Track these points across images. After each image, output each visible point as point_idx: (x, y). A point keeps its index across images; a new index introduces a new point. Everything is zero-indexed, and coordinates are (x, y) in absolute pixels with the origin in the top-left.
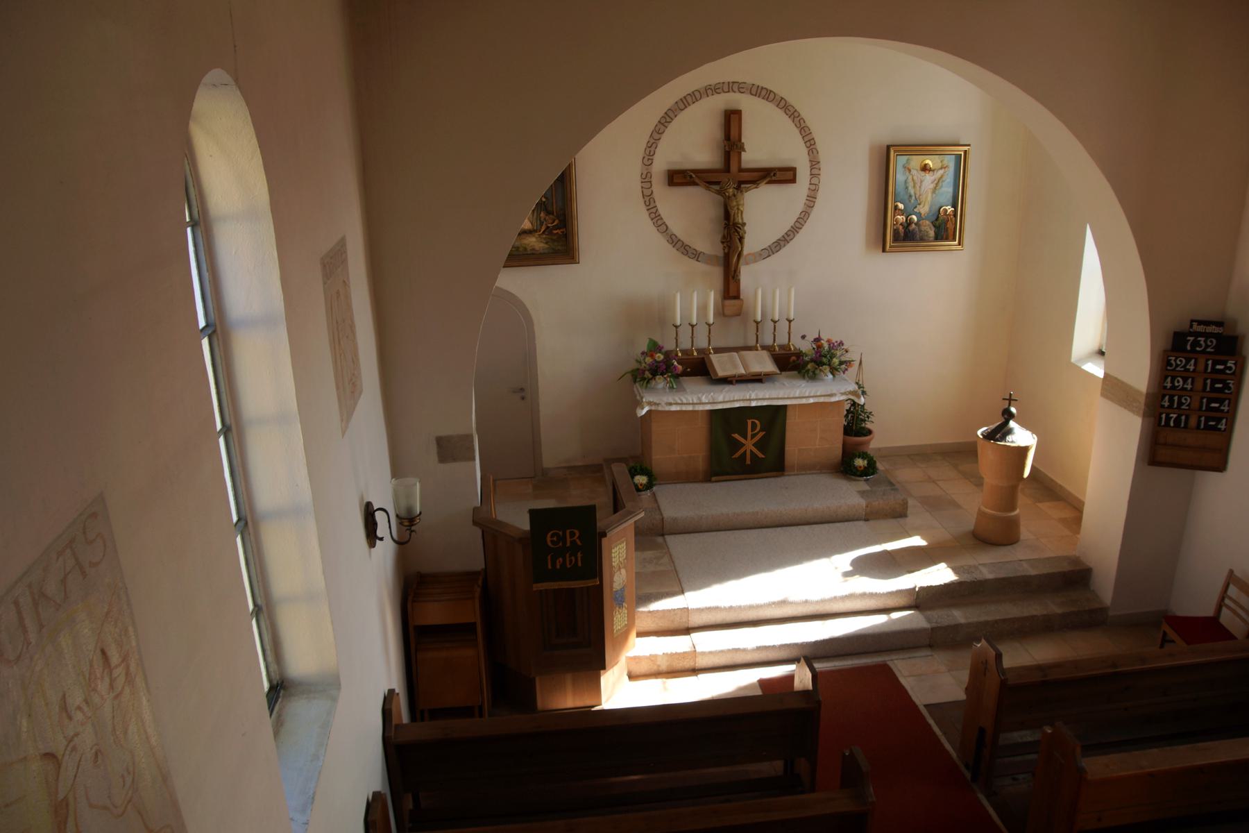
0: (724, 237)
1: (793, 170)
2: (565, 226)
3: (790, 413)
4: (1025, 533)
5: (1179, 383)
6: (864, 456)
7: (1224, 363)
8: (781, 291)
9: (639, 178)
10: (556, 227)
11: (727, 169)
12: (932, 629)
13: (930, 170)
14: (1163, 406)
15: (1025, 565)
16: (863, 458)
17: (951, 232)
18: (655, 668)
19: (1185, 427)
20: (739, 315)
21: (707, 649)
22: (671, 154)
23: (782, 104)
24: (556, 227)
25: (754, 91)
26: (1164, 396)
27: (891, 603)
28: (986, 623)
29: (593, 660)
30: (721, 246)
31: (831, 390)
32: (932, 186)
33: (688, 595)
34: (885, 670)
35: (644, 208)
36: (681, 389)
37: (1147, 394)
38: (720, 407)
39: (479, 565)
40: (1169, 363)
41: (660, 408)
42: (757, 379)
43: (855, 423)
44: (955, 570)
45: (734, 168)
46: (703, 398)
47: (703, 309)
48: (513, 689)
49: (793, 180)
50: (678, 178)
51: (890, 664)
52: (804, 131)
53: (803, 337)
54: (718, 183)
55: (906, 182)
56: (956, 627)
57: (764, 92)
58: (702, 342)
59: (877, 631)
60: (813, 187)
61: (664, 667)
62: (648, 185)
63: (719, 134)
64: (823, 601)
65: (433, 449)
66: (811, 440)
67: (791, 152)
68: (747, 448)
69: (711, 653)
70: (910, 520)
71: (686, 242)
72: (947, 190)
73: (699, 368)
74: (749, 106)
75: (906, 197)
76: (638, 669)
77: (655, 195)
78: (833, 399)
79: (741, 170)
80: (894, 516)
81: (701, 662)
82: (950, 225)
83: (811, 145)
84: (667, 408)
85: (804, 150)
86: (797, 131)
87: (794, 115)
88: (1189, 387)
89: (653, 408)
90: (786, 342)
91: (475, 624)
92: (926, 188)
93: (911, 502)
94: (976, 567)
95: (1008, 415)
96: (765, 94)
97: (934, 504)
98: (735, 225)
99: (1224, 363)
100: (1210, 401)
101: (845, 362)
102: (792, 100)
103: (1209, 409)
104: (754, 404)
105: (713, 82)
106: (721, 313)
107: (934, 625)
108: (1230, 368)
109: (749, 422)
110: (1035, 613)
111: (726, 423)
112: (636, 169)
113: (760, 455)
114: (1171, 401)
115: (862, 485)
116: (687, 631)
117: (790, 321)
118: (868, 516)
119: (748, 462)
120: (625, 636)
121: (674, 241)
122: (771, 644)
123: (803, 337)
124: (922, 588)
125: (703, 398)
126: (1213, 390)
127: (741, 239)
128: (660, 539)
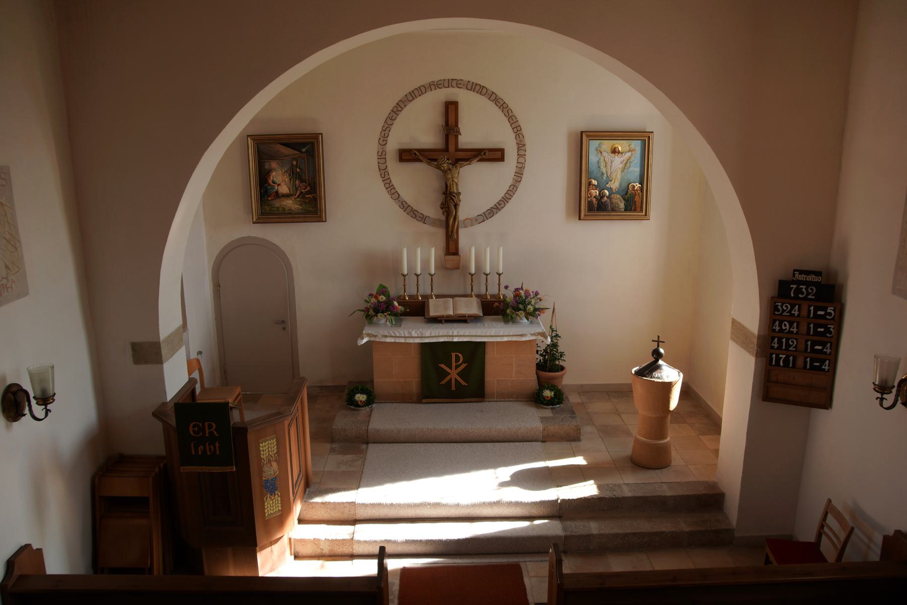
0: (442, 204)
1: (502, 151)
2: (315, 192)
3: (488, 350)
4: (677, 457)
5: (786, 326)
6: (552, 388)
7: (825, 309)
8: (491, 250)
9: (376, 157)
10: (308, 193)
11: (446, 149)
12: (566, 537)
13: (619, 152)
14: (773, 348)
15: (665, 487)
16: (551, 390)
17: (638, 204)
18: (318, 551)
19: (794, 366)
20: (458, 268)
21: (362, 539)
22: (399, 138)
23: (493, 97)
24: (308, 193)
25: (469, 87)
26: (773, 338)
27: (535, 512)
28: (617, 535)
29: (247, 538)
30: (441, 211)
31: (523, 331)
32: (621, 166)
33: (362, 490)
34: (516, 572)
35: (380, 180)
36: (398, 324)
37: (758, 336)
38: (427, 341)
39: (162, 451)
40: (776, 308)
41: (377, 340)
42: (462, 320)
43: (550, 362)
44: (599, 487)
45: (452, 148)
46: (418, 333)
47: (426, 263)
48: (184, 558)
49: (501, 159)
50: (407, 155)
51: (522, 565)
52: (512, 119)
53: (506, 287)
54: (435, 160)
55: (598, 162)
56: (589, 537)
57: (477, 88)
58: (425, 289)
59: (502, 535)
60: (520, 165)
61: (326, 551)
62: (382, 161)
63: (440, 121)
64: (474, 505)
65: (129, 352)
66: (508, 371)
67: (503, 137)
68: (453, 377)
69: (365, 542)
70: (583, 444)
71: (415, 208)
72: (635, 170)
73: (417, 309)
74: (464, 97)
75: (599, 175)
76: (303, 550)
77: (389, 169)
78: (524, 339)
79: (457, 150)
80: (570, 440)
81: (358, 550)
82: (637, 199)
83: (517, 130)
84: (383, 340)
85: (512, 135)
86: (505, 120)
87: (503, 107)
88: (795, 330)
89: (372, 339)
90: (496, 292)
91: (148, 498)
92: (616, 167)
93: (587, 429)
94: (619, 486)
95: (657, 355)
96: (478, 89)
97: (607, 432)
98: (451, 193)
99: (825, 309)
100: (814, 343)
101: (539, 309)
102: (500, 94)
103: (814, 351)
104: (456, 340)
105: (436, 78)
106: (442, 267)
107: (569, 533)
108: (830, 314)
109: (453, 355)
110: (664, 530)
111: (434, 353)
112: (373, 148)
113: (464, 383)
114: (780, 342)
115: (547, 412)
116: (354, 522)
117: (499, 275)
118: (546, 438)
119: (453, 388)
120: (281, 520)
121: (405, 206)
122: (419, 539)
123: (506, 287)
124: (563, 500)
125: (418, 333)
126: (816, 333)
127: (456, 206)
128: (364, 446)
